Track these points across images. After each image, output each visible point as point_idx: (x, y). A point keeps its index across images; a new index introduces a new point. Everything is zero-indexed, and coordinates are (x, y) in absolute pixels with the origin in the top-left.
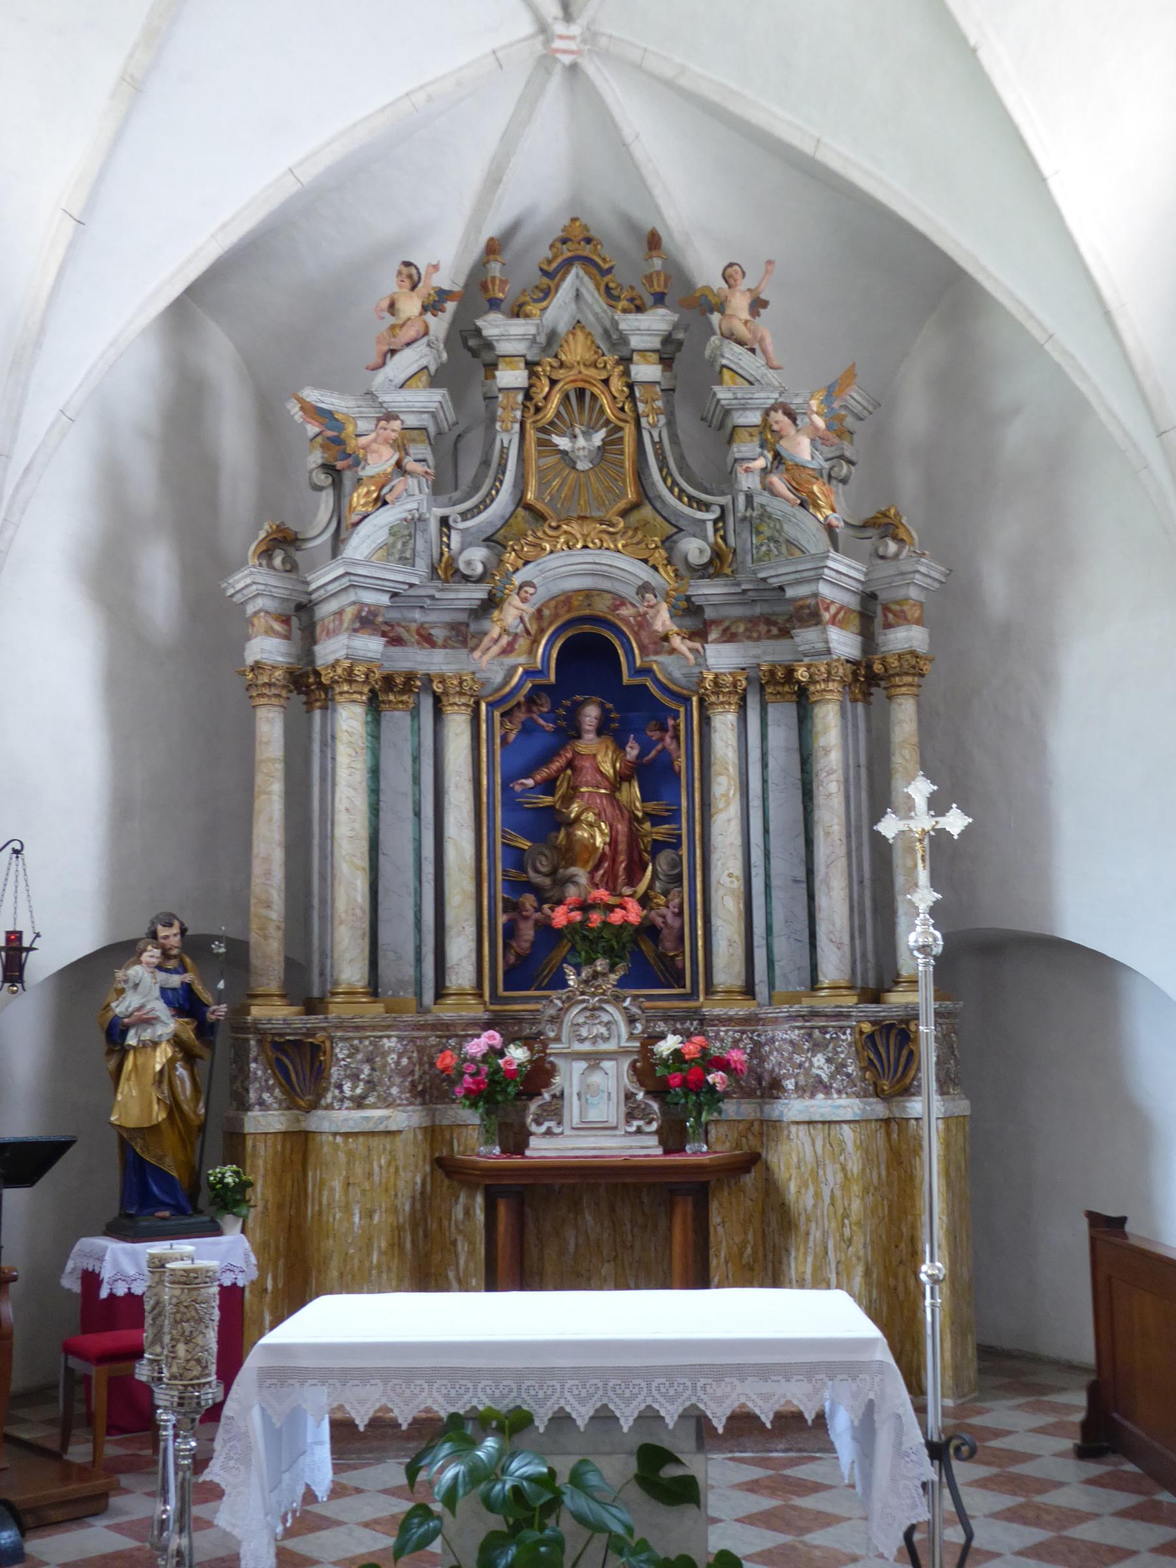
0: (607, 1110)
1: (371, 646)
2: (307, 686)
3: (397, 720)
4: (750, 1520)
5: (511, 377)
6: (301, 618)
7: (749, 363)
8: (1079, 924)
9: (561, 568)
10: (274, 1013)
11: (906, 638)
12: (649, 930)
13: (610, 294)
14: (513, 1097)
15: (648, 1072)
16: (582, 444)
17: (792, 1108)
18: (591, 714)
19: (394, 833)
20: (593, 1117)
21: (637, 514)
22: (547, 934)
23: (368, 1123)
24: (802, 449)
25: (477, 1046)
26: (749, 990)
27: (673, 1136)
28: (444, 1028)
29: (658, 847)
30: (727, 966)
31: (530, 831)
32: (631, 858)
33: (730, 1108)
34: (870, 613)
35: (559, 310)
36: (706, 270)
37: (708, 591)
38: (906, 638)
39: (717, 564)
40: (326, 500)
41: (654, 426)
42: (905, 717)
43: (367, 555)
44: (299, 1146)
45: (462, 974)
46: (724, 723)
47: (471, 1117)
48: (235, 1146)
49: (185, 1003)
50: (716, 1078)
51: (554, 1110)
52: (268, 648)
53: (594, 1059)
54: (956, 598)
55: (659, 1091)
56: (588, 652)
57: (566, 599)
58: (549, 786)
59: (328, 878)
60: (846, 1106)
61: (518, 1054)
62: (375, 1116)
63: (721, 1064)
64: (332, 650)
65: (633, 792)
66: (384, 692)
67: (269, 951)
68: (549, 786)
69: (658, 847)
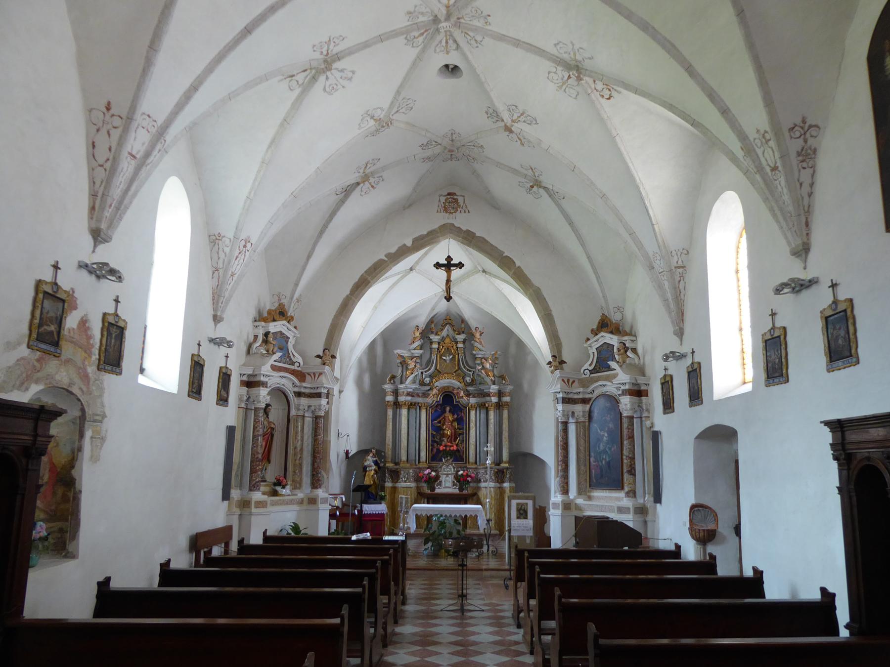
0: (449, 484)
1: (409, 398)
2: (397, 405)
3: (412, 411)
4: (490, 633)
5: (435, 346)
6: (396, 393)
7: (479, 346)
8: (537, 452)
9: (443, 382)
10: (390, 465)
11: (506, 399)
12: (458, 451)
13: (454, 331)
14: (432, 481)
15: (457, 477)
16: (448, 358)
17: (483, 485)
18: (448, 409)
19: (411, 432)
20: (447, 485)
21: (459, 374)
22: (438, 450)
23: (406, 485)
24: (488, 366)
25: (426, 472)
26: (476, 463)
27: (461, 489)
28: (420, 469)
29: (460, 434)
30: (472, 459)
31: (436, 432)
32: (455, 436)
33: (472, 484)
34: (500, 394)
35: (444, 333)
36: (473, 324)
37: (470, 388)
38: (506, 399)
39: (472, 383)
40: (400, 369)
41: (461, 356)
42: (505, 413)
43: (409, 385)
44: (394, 489)
45: (423, 458)
46: (473, 413)
47: (425, 485)
48: (383, 488)
49: (376, 463)
50: (469, 479)
51: (440, 484)
52: (390, 398)
53: (447, 475)
54: (518, 386)
55: (459, 481)
56: (448, 397)
57: (444, 387)
58: (439, 422)
59: (400, 441)
60: (492, 484)
61: (434, 474)
62: (408, 484)
63: (470, 476)
64: (402, 399)
65: (455, 424)
66: (411, 406)
67: (389, 453)
68: (439, 422)
69: (460, 434)
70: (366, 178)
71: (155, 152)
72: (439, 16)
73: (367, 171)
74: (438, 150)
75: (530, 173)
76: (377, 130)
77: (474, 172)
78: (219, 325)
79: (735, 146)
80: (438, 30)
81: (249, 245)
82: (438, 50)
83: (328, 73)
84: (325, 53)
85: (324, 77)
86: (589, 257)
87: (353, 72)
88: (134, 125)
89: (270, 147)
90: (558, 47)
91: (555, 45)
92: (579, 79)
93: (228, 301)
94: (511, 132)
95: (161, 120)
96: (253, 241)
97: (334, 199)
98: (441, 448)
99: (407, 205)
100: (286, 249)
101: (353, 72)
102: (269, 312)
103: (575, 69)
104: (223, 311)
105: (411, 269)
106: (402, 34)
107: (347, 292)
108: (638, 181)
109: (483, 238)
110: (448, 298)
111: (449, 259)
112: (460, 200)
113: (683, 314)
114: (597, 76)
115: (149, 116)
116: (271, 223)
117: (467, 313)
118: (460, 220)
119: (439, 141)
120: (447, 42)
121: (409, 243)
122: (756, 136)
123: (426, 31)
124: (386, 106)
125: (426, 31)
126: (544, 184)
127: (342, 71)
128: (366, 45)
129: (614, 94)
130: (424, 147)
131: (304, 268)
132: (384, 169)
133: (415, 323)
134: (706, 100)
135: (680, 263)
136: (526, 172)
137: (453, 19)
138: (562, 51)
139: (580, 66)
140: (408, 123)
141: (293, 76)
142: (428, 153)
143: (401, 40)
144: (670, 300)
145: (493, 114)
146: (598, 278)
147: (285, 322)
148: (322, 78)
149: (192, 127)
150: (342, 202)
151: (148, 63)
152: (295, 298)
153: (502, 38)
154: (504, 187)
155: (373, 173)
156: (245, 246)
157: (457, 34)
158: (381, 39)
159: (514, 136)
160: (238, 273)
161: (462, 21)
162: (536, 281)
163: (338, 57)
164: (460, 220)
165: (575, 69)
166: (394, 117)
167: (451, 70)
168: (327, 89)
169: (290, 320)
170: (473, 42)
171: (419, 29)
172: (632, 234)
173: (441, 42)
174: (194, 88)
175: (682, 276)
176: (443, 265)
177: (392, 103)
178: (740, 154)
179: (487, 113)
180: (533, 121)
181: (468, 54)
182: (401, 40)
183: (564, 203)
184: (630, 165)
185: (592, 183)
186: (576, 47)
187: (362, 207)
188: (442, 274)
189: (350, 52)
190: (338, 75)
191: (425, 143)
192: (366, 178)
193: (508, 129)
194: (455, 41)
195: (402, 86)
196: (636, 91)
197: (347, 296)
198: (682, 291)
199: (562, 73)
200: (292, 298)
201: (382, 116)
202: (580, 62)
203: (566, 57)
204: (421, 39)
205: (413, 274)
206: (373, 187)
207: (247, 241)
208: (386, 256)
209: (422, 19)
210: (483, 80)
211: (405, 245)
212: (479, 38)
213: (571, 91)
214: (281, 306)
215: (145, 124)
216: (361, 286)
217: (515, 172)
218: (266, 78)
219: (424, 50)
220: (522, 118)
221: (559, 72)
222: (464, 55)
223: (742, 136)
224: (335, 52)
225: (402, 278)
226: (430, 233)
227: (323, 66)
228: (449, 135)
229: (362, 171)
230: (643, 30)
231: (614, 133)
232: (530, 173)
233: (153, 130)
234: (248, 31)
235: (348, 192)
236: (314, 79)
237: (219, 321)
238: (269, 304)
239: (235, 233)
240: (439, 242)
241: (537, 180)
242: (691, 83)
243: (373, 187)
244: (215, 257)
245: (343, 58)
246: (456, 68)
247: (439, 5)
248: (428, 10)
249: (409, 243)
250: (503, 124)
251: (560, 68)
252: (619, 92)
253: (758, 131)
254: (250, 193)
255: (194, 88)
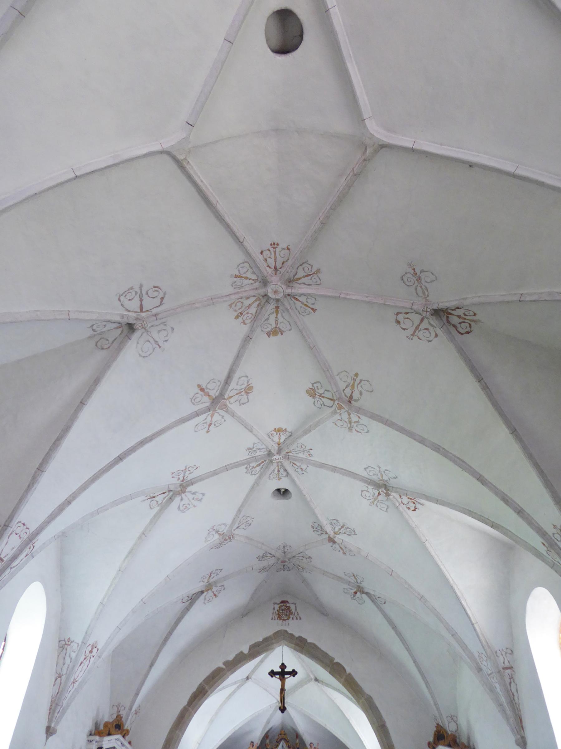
70: (209, 587)
71: (22, 556)
72: (272, 451)
73: (211, 581)
74: (272, 561)
75: (352, 580)
76: (221, 544)
77: (304, 581)
78: (51, 738)
79: (536, 541)
80: (271, 461)
81: (95, 650)
82: (272, 477)
83: (183, 495)
84: (181, 479)
85: (180, 498)
86: (415, 662)
87: (203, 495)
88: (9, 530)
89: (127, 557)
90: (368, 470)
91: (365, 469)
92: (388, 495)
93: (64, 711)
94: (334, 542)
95: (33, 528)
96: (100, 647)
97: (180, 606)
99: (245, 613)
100: (132, 657)
101: (203, 495)
102: (106, 725)
103: (384, 487)
104: (57, 723)
105: (248, 678)
106: (244, 464)
107: (185, 702)
108: (452, 582)
109: (314, 645)
110: (283, 709)
111: (283, 666)
112: (292, 607)
113: (521, 720)
114: (403, 492)
115: (24, 524)
116: (119, 628)
117: (302, 727)
118: (293, 627)
119: (273, 553)
120: (279, 471)
121: (246, 651)
122: (555, 531)
123: (262, 462)
124: (229, 522)
125: (262, 462)
126: (366, 590)
127: (194, 493)
128: (215, 473)
129: (418, 506)
130: (260, 558)
131: (146, 676)
132: (225, 578)
133: (250, 738)
134: (501, 503)
135: (507, 664)
136: (349, 579)
137: (284, 453)
138: (371, 474)
139: (387, 484)
140: (247, 538)
141: (154, 497)
142: (264, 564)
143: (243, 469)
144: (505, 704)
145: (319, 528)
146: (427, 683)
147: (119, 736)
148: (177, 499)
149: (63, 535)
150: (188, 609)
151: (34, 480)
152: (133, 709)
153: (322, 466)
154: (331, 594)
155: (215, 583)
156: (91, 652)
157: (287, 464)
158: (227, 468)
159: (336, 546)
160: (80, 679)
161: (290, 454)
162: (367, 687)
163: (192, 483)
164: (293, 627)
165: (384, 487)
166: (236, 532)
167: (283, 493)
168: (181, 508)
169: (125, 734)
170: (299, 470)
171: (256, 461)
172: (454, 635)
173: (274, 470)
174: (68, 502)
175: (511, 678)
176: (277, 673)
177: (234, 519)
178: (543, 550)
179: (313, 527)
180: (352, 533)
181: (296, 479)
182: (243, 469)
183: (386, 607)
184: (442, 567)
185: (409, 585)
186: (383, 469)
187: (204, 615)
188: (276, 682)
189: (201, 478)
190: (191, 496)
191: (261, 555)
192: (209, 588)
193: (332, 540)
194: (285, 470)
195: (242, 505)
196: (437, 502)
197: (185, 707)
198: (515, 694)
199: (372, 491)
200: (131, 709)
201: (225, 531)
202: (386, 481)
203: (375, 478)
204: (258, 469)
205: (249, 683)
206: (215, 595)
207: (93, 646)
208: (224, 664)
209: (259, 453)
210: (309, 499)
211: (242, 652)
212: (304, 467)
213: (383, 505)
214: (119, 717)
215: (18, 531)
216: (199, 695)
217: (339, 579)
218: (131, 497)
219: (260, 477)
220: (343, 531)
221: (370, 490)
222: (293, 481)
223: (542, 533)
224: (189, 478)
225: (238, 688)
226: (266, 640)
227: (179, 489)
228: (282, 548)
229: (206, 580)
230: (436, 451)
231: (423, 539)
232: (352, 580)
233: (25, 537)
234: (120, 458)
235: (193, 599)
236: (171, 499)
237: (52, 734)
238: (107, 717)
239: (84, 638)
240: (273, 649)
241: (359, 587)
242: (484, 489)
243: (215, 595)
244: (61, 662)
245: (196, 483)
246: (286, 491)
247: (272, 443)
248: (264, 446)
249: (246, 651)
250: (327, 536)
251: (370, 487)
252: (423, 505)
253: (555, 526)
254: (104, 598)
255: (68, 502)
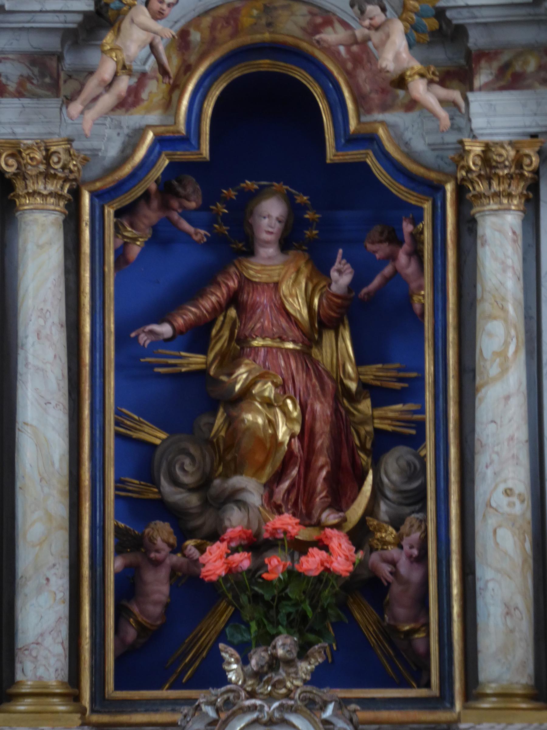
12: (367, 586)
18: (271, 213)
22: (190, 585)
29: (384, 441)
31: (167, 411)
32: (338, 460)
58: (198, 337)
65: (340, 349)
68: (198, 337)
69: (384, 441)
98: (214, 562)
